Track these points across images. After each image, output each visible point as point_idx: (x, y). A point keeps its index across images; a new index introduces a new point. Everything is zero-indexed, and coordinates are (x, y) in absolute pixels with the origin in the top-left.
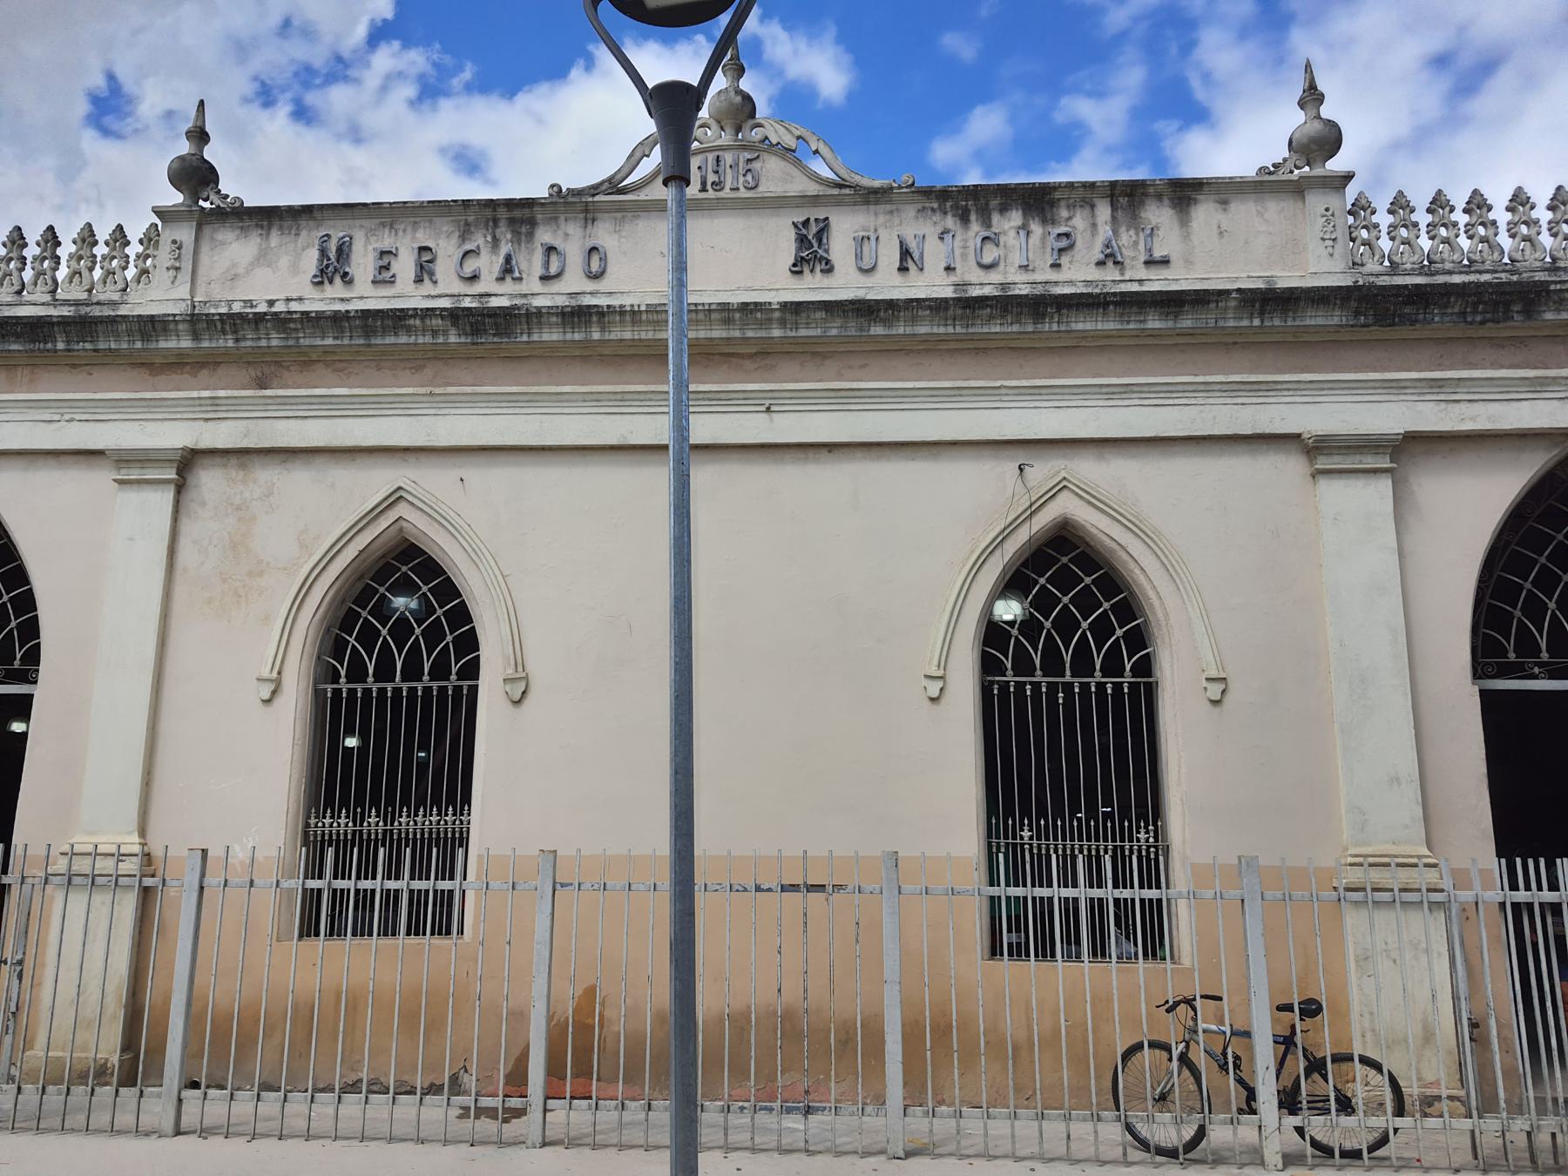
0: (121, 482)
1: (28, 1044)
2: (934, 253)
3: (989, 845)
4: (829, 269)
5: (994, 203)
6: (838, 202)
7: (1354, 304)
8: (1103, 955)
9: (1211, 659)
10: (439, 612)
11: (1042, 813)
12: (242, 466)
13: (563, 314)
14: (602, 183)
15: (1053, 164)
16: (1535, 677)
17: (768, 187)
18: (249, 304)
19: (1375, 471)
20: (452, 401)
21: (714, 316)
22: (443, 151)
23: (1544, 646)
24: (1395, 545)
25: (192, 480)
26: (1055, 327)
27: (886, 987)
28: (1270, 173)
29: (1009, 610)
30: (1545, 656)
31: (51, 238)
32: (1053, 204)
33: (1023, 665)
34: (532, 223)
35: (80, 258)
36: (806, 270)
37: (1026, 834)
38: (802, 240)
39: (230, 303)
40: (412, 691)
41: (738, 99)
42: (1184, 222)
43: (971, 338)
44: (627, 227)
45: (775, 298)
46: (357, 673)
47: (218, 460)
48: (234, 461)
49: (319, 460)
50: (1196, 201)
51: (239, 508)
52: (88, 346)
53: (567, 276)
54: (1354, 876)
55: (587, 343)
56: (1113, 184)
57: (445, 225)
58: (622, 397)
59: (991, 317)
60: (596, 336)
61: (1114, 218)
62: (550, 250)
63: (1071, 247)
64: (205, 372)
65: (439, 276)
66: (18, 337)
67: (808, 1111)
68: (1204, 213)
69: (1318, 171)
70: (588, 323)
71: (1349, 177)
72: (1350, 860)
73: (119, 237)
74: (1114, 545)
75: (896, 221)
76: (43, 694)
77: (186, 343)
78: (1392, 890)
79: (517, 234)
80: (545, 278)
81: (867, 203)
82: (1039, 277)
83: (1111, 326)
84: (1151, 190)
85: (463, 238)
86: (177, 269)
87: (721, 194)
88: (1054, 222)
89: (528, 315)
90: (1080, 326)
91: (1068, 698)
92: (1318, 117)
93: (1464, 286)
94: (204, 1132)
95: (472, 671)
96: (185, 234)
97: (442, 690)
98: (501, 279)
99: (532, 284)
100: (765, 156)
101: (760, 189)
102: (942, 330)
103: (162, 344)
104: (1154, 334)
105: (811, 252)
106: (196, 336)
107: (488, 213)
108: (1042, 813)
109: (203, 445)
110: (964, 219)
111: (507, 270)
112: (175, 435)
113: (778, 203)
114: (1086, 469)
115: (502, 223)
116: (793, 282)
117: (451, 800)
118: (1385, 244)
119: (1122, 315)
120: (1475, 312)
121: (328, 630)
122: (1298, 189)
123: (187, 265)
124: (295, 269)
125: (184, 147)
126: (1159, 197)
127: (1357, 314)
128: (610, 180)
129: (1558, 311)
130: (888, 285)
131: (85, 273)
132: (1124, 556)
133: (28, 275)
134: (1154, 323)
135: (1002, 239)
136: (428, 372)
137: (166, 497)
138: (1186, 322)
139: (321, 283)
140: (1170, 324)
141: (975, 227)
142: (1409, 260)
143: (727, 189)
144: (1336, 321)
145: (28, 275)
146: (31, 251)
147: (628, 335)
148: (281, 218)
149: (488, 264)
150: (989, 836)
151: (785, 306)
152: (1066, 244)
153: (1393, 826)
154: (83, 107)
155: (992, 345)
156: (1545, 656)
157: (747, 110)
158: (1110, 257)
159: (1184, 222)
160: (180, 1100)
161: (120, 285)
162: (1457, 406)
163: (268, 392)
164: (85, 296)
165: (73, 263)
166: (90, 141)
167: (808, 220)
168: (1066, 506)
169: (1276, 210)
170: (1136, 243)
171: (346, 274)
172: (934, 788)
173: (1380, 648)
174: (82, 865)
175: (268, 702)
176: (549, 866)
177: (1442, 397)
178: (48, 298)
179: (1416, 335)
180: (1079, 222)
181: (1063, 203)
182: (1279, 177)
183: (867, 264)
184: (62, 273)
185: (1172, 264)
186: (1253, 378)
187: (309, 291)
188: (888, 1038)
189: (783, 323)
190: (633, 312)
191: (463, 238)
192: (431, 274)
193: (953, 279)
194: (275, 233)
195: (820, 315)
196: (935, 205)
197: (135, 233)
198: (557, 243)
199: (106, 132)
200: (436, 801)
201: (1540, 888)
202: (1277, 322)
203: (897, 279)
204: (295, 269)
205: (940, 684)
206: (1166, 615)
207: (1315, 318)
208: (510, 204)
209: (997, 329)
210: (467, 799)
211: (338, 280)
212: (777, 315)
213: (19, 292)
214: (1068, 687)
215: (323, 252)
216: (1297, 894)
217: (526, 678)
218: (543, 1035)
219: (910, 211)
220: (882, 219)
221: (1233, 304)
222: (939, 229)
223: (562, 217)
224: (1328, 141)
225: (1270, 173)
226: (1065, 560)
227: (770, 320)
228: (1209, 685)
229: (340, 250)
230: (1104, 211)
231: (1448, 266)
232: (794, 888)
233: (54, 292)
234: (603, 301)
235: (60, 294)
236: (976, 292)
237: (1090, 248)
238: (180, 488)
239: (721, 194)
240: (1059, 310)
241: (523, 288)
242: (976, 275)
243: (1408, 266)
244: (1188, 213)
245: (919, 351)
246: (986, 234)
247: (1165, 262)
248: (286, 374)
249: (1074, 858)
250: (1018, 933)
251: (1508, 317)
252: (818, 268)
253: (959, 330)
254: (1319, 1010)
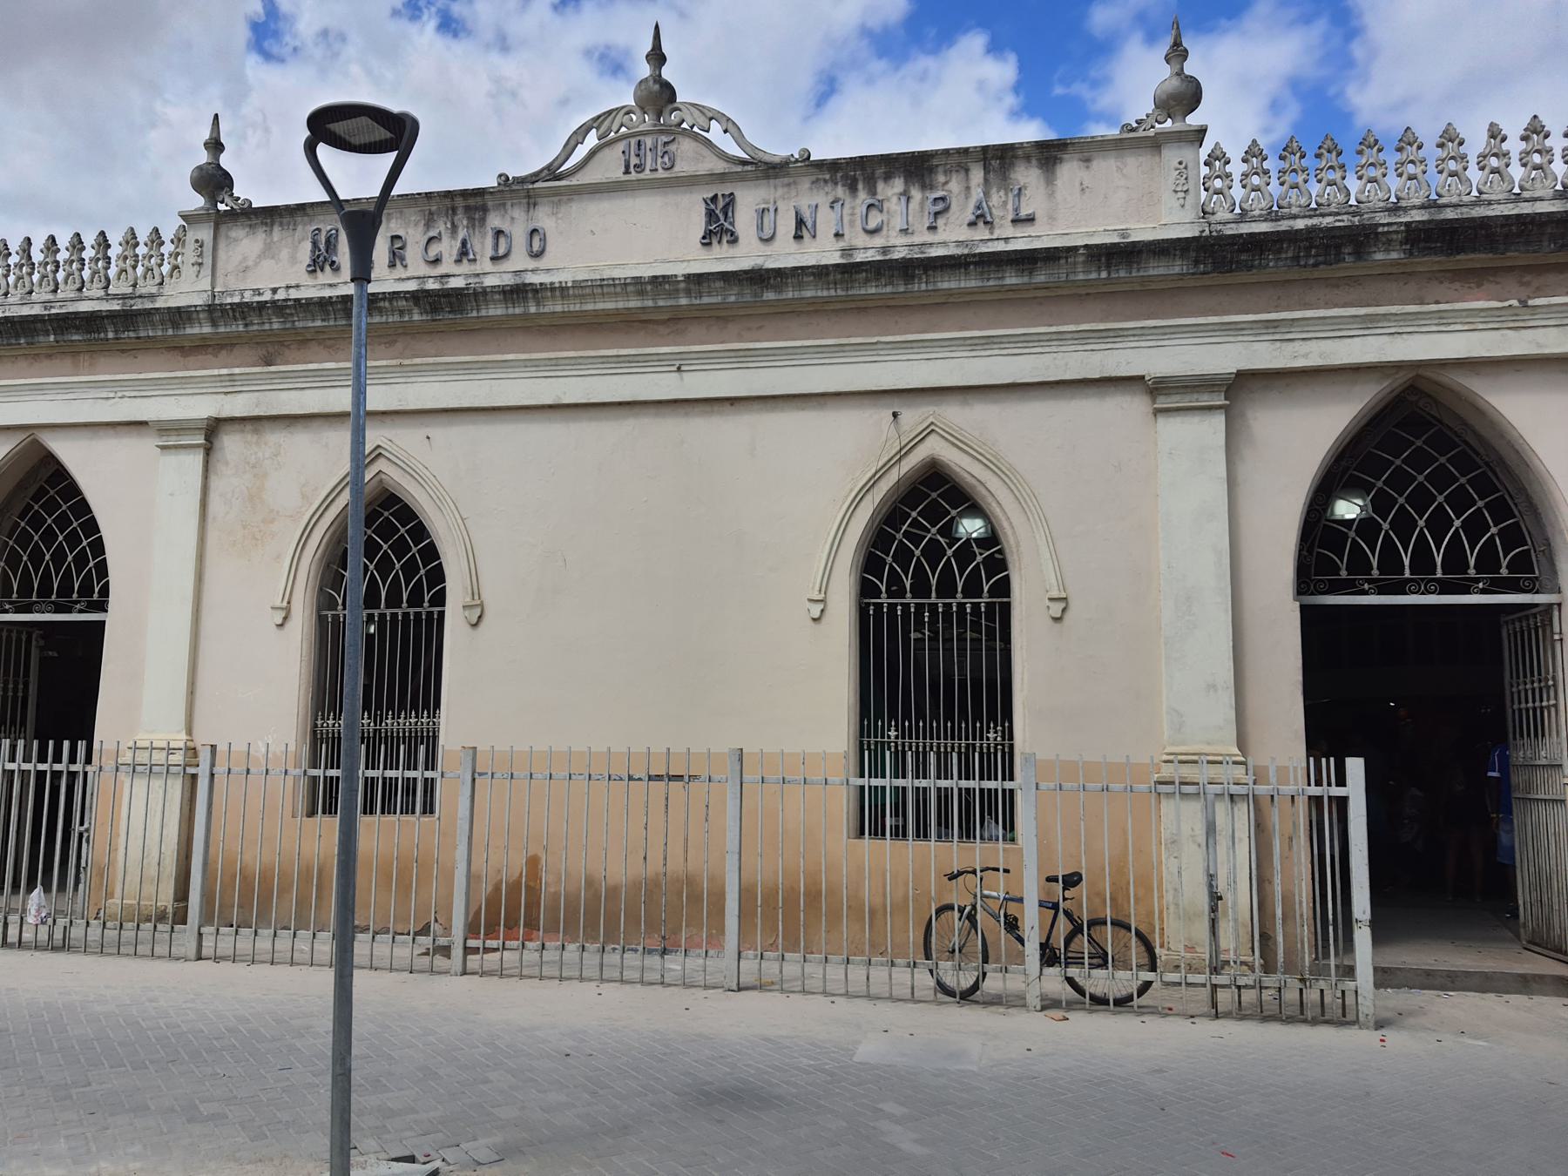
0: (163, 448)
1: (109, 895)
2: (826, 221)
3: (861, 743)
4: (734, 240)
5: (880, 172)
6: (741, 178)
7: (1193, 254)
8: (925, 836)
9: (1054, 581)
10: (414, 550)
11: (907, 716)
12: (256, 431)
13: (504, 292)
14: (542, 170)
15: (1223, 22)
16: (1365, 593)
17: (683, 168)
18: (258, 292)
19: (1210, 408)
20: (419, 370)
21: (630, 288)
22: (588, 53)
23: (1375, 564)
24: (1224, 474)
25: (217, 444)
26: (923, 287)
27: (728, 856)
28: (1133, 130)
29: (971, 527)
30: (1375, 572)
31: (77, 243)
32: (932, 170)
33: (896, 590)
34: (484, 210)
35: (126, 258)
36: (715, 241)
37: (893, 733)
38: (711, 215)
39: (242, 292)
40: (394, 616)
41: (657, 87)
42: (1050, 179)
43: (852, 299)
44: (563, 209)
45: (680, 270)
46: (896, 590)
47: (237, 426)
48: (249, 427)
49: (316, 424)
50: (1061, 160)
51: (254, 467)
52: (132, 334)
53: (513, 256)
54: (1167, 772)
55: (526, 316)
56: (985, 149)
57: (413, 215)
58: (555, 363)
59: (867, 280)
60: (533, 310)
61: (986, 180)
62: (499, 233)
63: (946, 209)
64: (224, 352)
65: (408, 261)
66: (77, 328)
67: (664, 952)
68: (1069, 171)
69: (1179, 126)
70: (525, 299)
71: (1202, 131)
72: (1165, 757)
73: (156, 238)
74: (973, 481)
75: (793, 193)
76: (116, 621)
77: (207, 329)
78: (1173, 783)
79: (471, 219)
80: (494, 259)
81: (768, 177)
82: (917, 239)
83: (973, 283)
84: (1020, 152)
85: (428, 226)
86: (200, 264)
87: (641, 176)
88: (932, 187)
89: (476, 294)
90: (945, 285)
91: (933, 621)
92: (1180, 73)
93: (1310, 230)
94: (217, 959)
95: (440, 599)
96: (205, 233)
97: (418, 615)
98: (458, 261)
99: (485, 265)
100: (680, 138)
101: (676, 169)
102: (825, 293)
103: (189, 331)
104: (1012, 289)
105: (718, 228)
106: (214, 324)
107: (448, 202)
108: (907, 716)
109: (224, 415)
110: (853, 189)
111: (464, 253)
112: (203, 407)
113: (691, 181)
114: (953, 414)
115: (460, 211)
116: (702, 253)
117: (426, 706)
118: (1237, 192)
119: (982, 273)
120: (1308, 256)
121: (328, 566)
122: (1156, 144)
123: (208, 261)
124: (293, 260)
125: (203, 157)
126: (1028, 158)
127: (1197, 262)
128: (548, 167)
129: (1387, 251)
130: (786, 254)
131: (130, 270)
132: (984, 492)
133: (86, 274)
134: (1011, 279)
135: (886, 205)
136: (399, 345)
137: (197, 459)
138: (1040, 278)
139: (314, 271)
140: (1026, 279)
141: (863, 196)
142: (1258, 205)
143: (647, 171)
144: (1177, 270)
145: (86, 274)
146: (88, 254)
147: (559, 308)
148: (281, 216)
149: (448, 248)
150: (862, 735)
151: (689, 278)
152: (942, 208)
153: (1205, 724)
154: (243, 34)
155: (871, 304)
156: (1375, 572)
157: (666, 95)
158: (981, 218)
159: (1050, 179)
160: (200, 935)
161: (157, 280)
162: (1291, 344)
163: (272, 368)
164: (130, 290)
165: (120, 263)
166: (254, 67)
167: (716, 196)
168: (934, 448)
169: (1134, 164)
170: (1005, 203)
171: (333, 263)
172: (806, 692)
173: (1205, 568)
174: (142, 757)
175: (281, 625)
176: (469, 759)
177: (1277, 337)
178: (101, 293)
179: (1254, 279)
180: (955, 185)
181: (940, 169)
182: (1140, 133)
183: (767, 233)
184: (112, 272)
185: (1037, 222)
186: (1102, 326)
187: (305, 279)
188: (728, 897)
189: (688, 292)
190: (562, 288)
191: (428, 226)
192: (402, 259)
193: (841, 244)
194: (276, 229)
195: (719, 284)
196: (828, 177)
197: (167, 234)
198: (505, 227)
199: (267, 56)
200: (415, 706)
201: (1329, 784)
202: (1122, 274)
203: (793, 246)
204: (293, 260)
205: (821, 606)
206: (1018, 545)
207: (1156, 269)
208: (465, 194)
209: (873, 291)
210: (437, 705)
211: (327, 268)
212: (682, 285)
213: (80, 290)
214: (933, 607)
215: (315, 244)
216: (1114, 786)
217: (482, 605)
218: (727, 938)
219: (805, 183)
220: (780, 191)
221: (1081, 259)
222: (831, 199)
223: (509, 206)
224: (1188, 96)
225: (1133, 130)
226: (934, 495)
227: (677, 290)
228: (1051, 604)
229: (328, 241)
230: (977, 175)
231: (1295, 210)
232: (659, 778)
233: (107, 287)
234: (545, 279)
235: (112, 290)
236: (859, 257)
237: (963, 209)
238: (208, 450)
239: (641, 176)
240: (925, 272)
241: (477, 268)
242: (861, 240)
243: (1257, 213)
244: (1053, 173)
245: (808, 312)
246: (871, 201)
247: (1030, 220)
248: (287, 352)
249: (904, 753)
250: (873, 818)
251: (1339, 260)
252: (725, 239)
253: (840, 292)
254: (1081, 879)
